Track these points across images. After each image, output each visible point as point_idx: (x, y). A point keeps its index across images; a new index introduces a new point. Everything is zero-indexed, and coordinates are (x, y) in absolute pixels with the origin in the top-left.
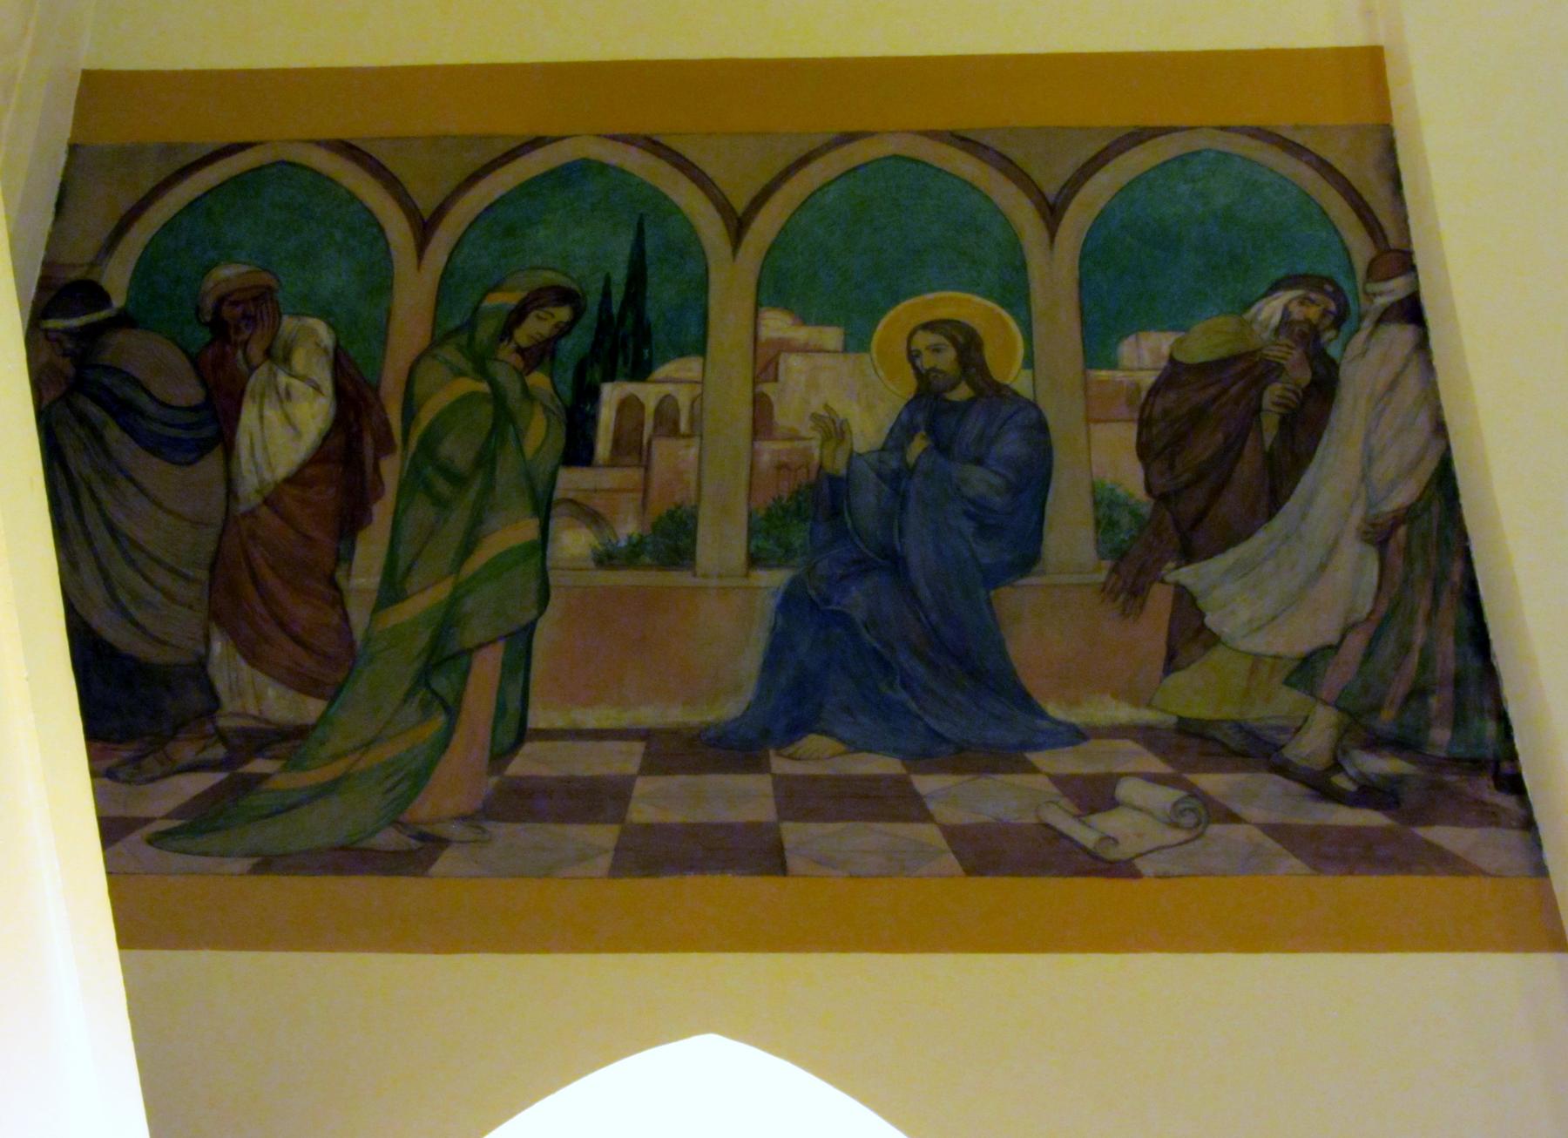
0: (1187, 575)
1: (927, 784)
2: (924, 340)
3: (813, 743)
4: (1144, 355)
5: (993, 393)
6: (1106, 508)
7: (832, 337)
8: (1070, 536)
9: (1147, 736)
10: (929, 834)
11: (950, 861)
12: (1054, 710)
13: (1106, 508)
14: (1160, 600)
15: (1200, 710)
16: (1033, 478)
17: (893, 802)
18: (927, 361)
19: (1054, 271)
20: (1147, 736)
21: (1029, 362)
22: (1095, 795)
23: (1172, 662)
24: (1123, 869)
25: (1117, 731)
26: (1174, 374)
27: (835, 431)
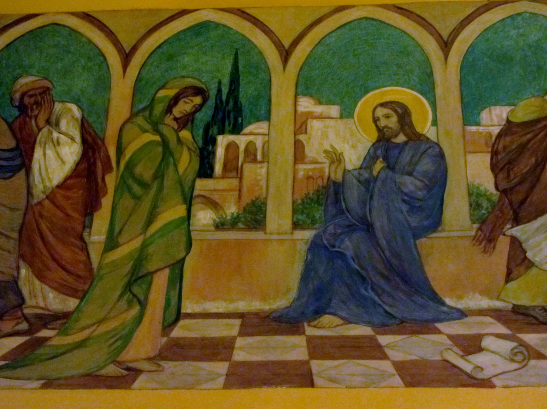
0: (517, 231)
1: (384, 340)
2: (381, 112)
3: (326, 319)
4: (494, 118)
5: (416, 138)
6: (475, 197)
7: (334, 110)
8: (457, 210)
9: (497, 314)
10: (386, 366)
11: (397, 380)
12: (449, 301)
13: (475, 197)
14: (503, 244)
15: (524, 301)
16: (438, 182)
17: (377, 352)
18: (383, 123)
19: (447, 76)
20: (497, 314)
21: (435, 122)
22: (471, 345)
23: (509, 277)
24: (486, 383)
25: (481, 312)
26: (510, 127)
27: (336, 158)
